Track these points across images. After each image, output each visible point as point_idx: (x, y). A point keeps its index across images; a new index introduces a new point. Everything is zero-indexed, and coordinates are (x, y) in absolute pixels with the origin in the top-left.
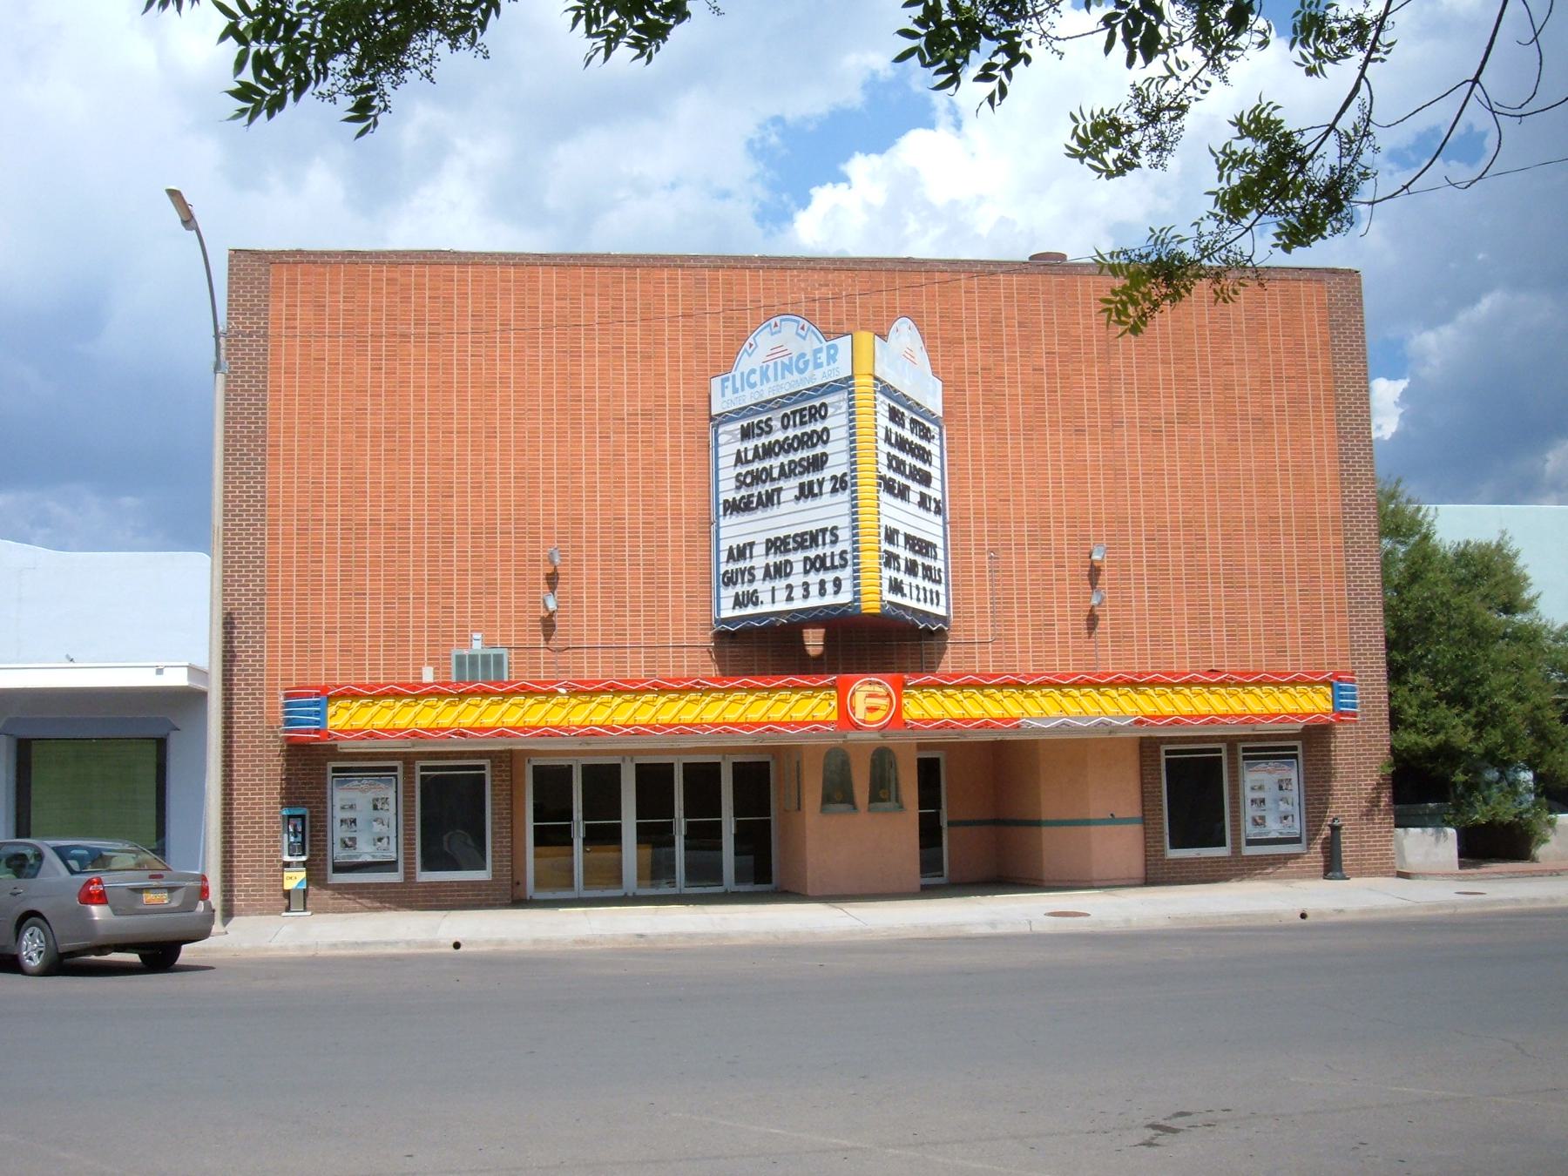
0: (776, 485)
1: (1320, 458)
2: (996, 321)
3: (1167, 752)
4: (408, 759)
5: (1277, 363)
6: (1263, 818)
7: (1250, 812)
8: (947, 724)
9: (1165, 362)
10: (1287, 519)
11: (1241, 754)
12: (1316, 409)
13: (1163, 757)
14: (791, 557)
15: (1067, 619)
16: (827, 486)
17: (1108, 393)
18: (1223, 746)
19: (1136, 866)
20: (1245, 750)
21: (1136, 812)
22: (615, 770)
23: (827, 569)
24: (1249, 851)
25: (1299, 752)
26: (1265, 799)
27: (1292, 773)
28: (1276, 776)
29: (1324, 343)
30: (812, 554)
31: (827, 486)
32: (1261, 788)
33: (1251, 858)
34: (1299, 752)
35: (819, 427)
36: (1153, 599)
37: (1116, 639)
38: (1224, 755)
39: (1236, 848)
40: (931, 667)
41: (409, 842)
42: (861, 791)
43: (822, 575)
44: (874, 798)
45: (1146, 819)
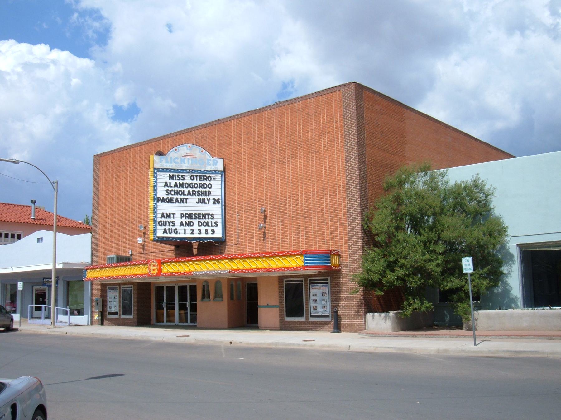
0: (186, 197)
1: (338, 162)
2: (241, 134)
3: (286, 282)
4: (119, 284)
5: (324, 128)
6: (316, 307)
7: (313, 304)
8: (182, 274)
9: (288, 136)
10: (326, 188)
11: (309, 282)
12: (337, 143)
13: (284, 283)
14: (193, 220)
15: (257, 235)
16: (212, 201)
17: (271, 152)
18: (303, 279)
19: (277, 324)
20: (310, 280)
21: (277, 304)
22: (163, 287)
23: (209, 226)
24: (312, 319)
25: (329, 281)
26: (318, 299)
27: (327, 289)
28: (321, 291)
29: (341, 115)
30: (202, 221)
31: (212, 201)
32: (316, 295)
33: (312, 322)
34: (329, 281)
35: (207, 182)
36: (283, 225)
37: (271, 240)
38: (303, 282)
39: (307, 318)
40: (222, 253)
41: (120, 307)
42: (212, 295)
43: (207, 228)
44: (215, 297)
45: (280, 306)
